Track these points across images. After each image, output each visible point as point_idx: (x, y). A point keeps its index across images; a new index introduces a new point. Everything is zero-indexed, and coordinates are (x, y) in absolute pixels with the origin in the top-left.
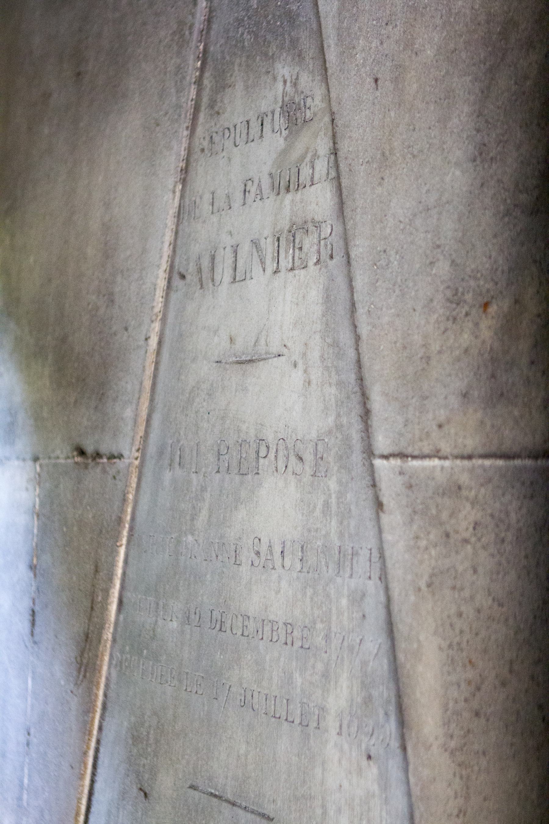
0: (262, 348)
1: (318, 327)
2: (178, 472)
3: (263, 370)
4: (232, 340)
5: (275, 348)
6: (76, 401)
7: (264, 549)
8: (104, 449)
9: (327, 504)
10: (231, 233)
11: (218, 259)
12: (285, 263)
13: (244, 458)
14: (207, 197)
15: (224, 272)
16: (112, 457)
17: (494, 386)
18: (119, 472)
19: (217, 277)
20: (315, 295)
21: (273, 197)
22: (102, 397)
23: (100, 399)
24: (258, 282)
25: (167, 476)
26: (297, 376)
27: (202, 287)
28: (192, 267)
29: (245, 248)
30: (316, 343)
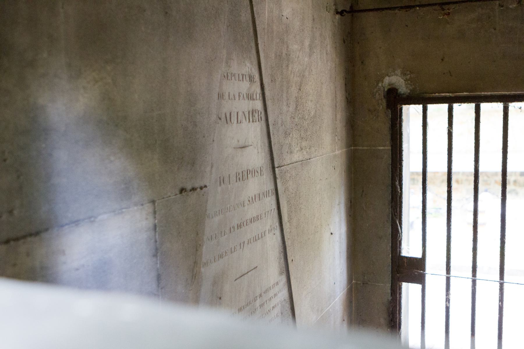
0: (247, 144)
2: (223, 185)
4: (238, 141)
5: (250, 144)
6: (178, 169)
8: (197, 185)
10: (236, 108)
13: (243, 176)
14: (227, 94)
16: (201, 188)
20: (258, 130)
22: (193, 164)
23: (193, 166)
25: (219, 189)
26: (256, 151)
28: (223, 116)
29: (240, 114)
30: (259, 141)
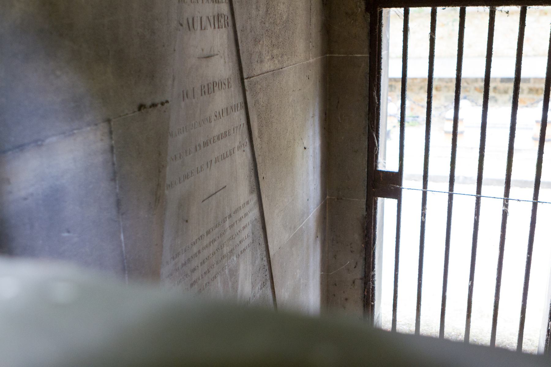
0: (212, 53)
1: (226, 46)
3: (214, 59)
4: (203, 50)
5: (216, 53)
7: (217, 114)
8: (157, 100)
9: (231, 95)
11: (195, 20)
12: (217, 26)
13: (209, 88)
15: (197, 25)
16: (162, 104)
17: (373, 276)
18: (166, 108)
19: (195, 27)
20: (225, 36)
21: (212, 3)
24: (210, 30)
25: (183, 104)
26: (222, 61)
27: (418, 117)
28: (185, 22)
29: (204, 19)
30: (226, 51)
